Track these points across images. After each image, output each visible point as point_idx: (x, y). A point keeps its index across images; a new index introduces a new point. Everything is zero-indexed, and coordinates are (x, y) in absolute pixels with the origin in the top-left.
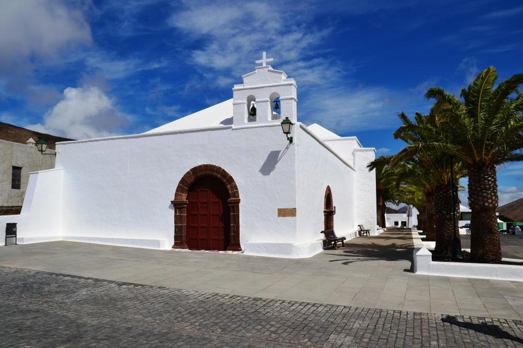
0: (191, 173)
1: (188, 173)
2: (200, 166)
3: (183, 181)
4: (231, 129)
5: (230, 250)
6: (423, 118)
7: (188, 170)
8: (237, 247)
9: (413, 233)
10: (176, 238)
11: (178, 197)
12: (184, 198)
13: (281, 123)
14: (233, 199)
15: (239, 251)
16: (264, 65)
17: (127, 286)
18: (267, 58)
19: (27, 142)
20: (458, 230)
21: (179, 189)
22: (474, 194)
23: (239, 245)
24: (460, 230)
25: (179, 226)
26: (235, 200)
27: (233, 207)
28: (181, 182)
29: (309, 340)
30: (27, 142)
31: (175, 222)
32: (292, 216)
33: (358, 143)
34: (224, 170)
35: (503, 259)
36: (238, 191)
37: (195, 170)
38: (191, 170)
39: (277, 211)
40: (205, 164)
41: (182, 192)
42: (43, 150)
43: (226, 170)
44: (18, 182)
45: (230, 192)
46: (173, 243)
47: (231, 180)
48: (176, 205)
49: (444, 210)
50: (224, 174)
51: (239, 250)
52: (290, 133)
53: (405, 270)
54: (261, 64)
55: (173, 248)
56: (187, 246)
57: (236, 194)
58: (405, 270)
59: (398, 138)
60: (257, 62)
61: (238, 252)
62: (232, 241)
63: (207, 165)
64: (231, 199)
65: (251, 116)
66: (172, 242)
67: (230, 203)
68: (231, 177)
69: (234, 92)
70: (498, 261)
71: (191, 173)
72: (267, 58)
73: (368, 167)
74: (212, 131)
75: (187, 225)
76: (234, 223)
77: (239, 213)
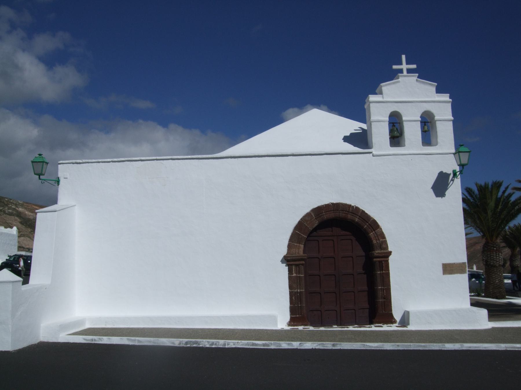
1: (308, 215)
3: (300, 226)
4: (372, 154)
7: (308, 210)
10: (293, 310)
12: (300, 250)
14: (379, 251)
17: (383, 294)
18: (401, 64)
21: (295, 238)
25: (297, 292)
27: (380, 262)
31: (290, 287)
36: (386, 241)
37: (318, 211)
40: (335, 202)
43: (366, 212)
45: (375, 242)
46: (288, 318)
48: (287, 260)
52: (44, 175)
55: (289, 324)
57: (383, 245)
59: (390, 251)
66: (287, 317)
68: (375, 222)
69: (437, 122)
72: (401, 64)
73: (407, 327)
74: (131, 162)
77: (389, 270)
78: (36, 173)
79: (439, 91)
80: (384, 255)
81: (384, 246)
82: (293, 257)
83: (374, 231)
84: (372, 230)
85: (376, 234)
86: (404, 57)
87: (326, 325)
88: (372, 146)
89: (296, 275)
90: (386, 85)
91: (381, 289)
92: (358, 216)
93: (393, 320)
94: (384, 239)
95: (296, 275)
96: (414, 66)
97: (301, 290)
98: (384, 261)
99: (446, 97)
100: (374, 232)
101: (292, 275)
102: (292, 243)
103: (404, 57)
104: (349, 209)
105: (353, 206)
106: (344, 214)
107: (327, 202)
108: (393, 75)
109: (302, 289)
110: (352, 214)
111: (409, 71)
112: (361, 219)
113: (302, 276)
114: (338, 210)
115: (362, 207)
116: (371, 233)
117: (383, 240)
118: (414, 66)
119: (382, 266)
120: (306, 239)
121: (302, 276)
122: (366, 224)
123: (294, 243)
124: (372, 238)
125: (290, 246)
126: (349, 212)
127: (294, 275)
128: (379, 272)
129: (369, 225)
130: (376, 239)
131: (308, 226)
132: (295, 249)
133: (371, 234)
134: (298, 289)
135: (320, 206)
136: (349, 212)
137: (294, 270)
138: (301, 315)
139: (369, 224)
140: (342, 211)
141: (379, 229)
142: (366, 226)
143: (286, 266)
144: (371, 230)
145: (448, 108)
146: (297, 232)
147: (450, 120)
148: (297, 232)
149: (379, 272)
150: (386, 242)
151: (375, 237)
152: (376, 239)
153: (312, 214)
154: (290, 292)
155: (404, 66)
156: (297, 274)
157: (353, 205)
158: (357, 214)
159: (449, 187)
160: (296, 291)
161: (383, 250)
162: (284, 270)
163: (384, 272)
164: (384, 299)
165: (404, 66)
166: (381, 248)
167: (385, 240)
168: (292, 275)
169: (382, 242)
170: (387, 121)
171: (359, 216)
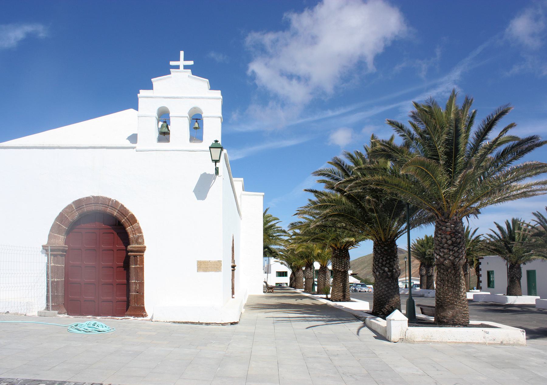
0: (74, 206)
1: (69, 207)
3: (61, 218)
4: (135, 150)
5: (131, 315)
6: (432, 238)
7: (70, 202)
8: (140, 311)
12: (60, 241)
13: (210, 148)
16: (182, 67)
18: (178, 60)
21: (55, 229)
22: (443, 248)
23: (143, 309)
27: (135, 256)
28: (58, 219)
32: (216, 271)
33: (511, 314)
34: (122, 206)
35: (471, 322)
38: (73, 202)
39: (196, 264)
40: (95, 196)
44: (493, 283)
45: (131, 236)
49: (386, 267)
51: (143, 316)
54: (177, 67)
56: (65, 311)
60: (172, 63)
61: (142, 318)
62: (133, 304)
63: (98, 197)
64: (134, 246)
65: (162, 136)
67: (132, 251)
68: (133, 217)
70: (466, 325)
71: (74, 206)
72: (178, 60)
75: (65, 280)
76: (137, 279)
78: (213, 159)
79: (213, 87)
80: (138, 250)
81: (140, 241)
82: (54, 247)
83: (132, 225)
84: (130, 224)
85: (133, 228)
86: (182, 53)
87: (84, 315)
88: (191, 143)
89: (53, 265)
90: (157, 80)
91: (135, 282)
92: (117, 209)
93: (144, 314)
94: (140, 233)
95: (53, 265)
96: (191, 63)
97: (58, 280)
98: (138, 255)
99: (218, 94)
100: (131, 226)
102: (53, 234)
103: (182, 53)
104: (109, 203)
105: (113, 200)
106: (103, 207)
108: (165, 71)
109: (62, 278)
110: (111, 208)
111: (186, 67)
112: (120, 213)
113: (59, 265)
114: (98, 204)
115: (121, 201)
116: (128, 228)
117: (140, 234)
118: (191, 63)
119: (137, 260)
120: (66, 230)
121: (59, 265)
122: (124, 218)
123: (54, 234)
124: (128, 232)
125: (50, 236)
126: (109, 206)
128: (133, 266)
129: (127, 219)
130: (133, 234)
131: (69, 218)
132: (55, 240)
133: (129, 229)
134: (55, 278)
136: (109, 206)
138: (57, 303)
139: (127, 218)
140: (102, 204)
141: (136, 224)
142: (124, 220)
143: (45, 256)
144: (129, 225)
145: (219, 104)
146: (57, 222)
147: (219, 117)
148: (57, 222)
149: (133, 266)
150: (142, 237)
151: (132, 231)
152: (133, 234)
153: (73, 206)
155: (182, 63)
158: (116, 208)
159: (212, 186)
160: (53, 280)
161: (138, 244)
162: (44, 259)
163: (138, 266)
164: (137, 293)
165: (182, 63)
166: (137, 243)
167: (141, 234)
169: (139, 237)
170: (154, 116)
171: (118, 210)
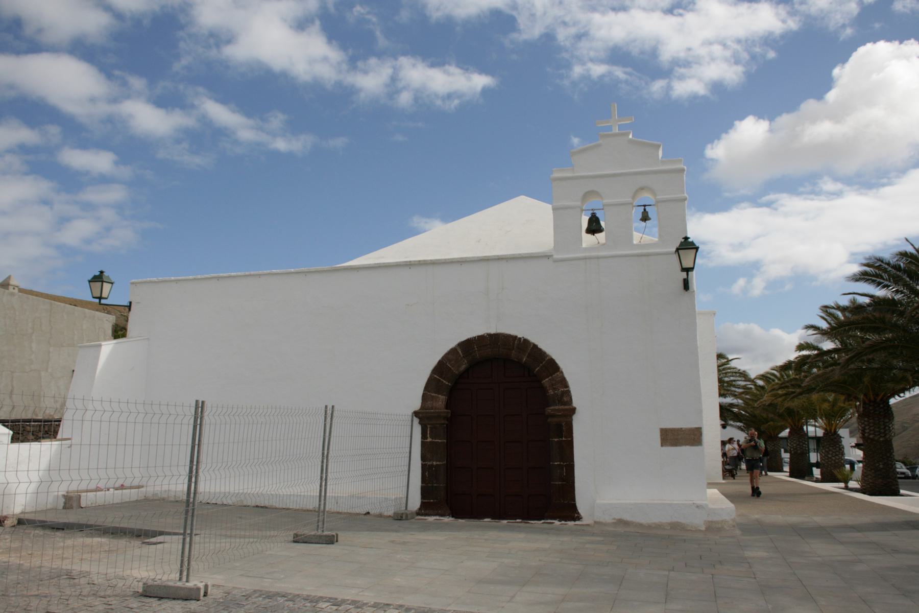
1: (453, 351)
2: (481, 338)
3: (441, 369)
7: (453, 344)
9: (207, 490)
11: (429, 403)
15: (575, 520)
19: (806, 432)
20: (790, 469)
21: (432, 386)
23: (574, 508)
24: (788, 470)
26: (563, 410)
29: (896, 340)
30: (806, 432)
34: (535, 346)
37: (467, 346)
39: (697, 426)
41: (438, 392)
42: (104, 295)
47: (552, 367)
50: (537, 354)
53: (852, 447)
58: (852, 447)
64: (557, 407)
101: (426, 440)
107: (480, 333)
115: (533, 339)
127: (429, 440)
135: (475, 337)
137: (428, 432)
146: (435, 376)
148: (435, 376)
154: (422, 464)
156: (432, 439)
157: (520, 336)
163: (564, 439)
168: (426, 440)
